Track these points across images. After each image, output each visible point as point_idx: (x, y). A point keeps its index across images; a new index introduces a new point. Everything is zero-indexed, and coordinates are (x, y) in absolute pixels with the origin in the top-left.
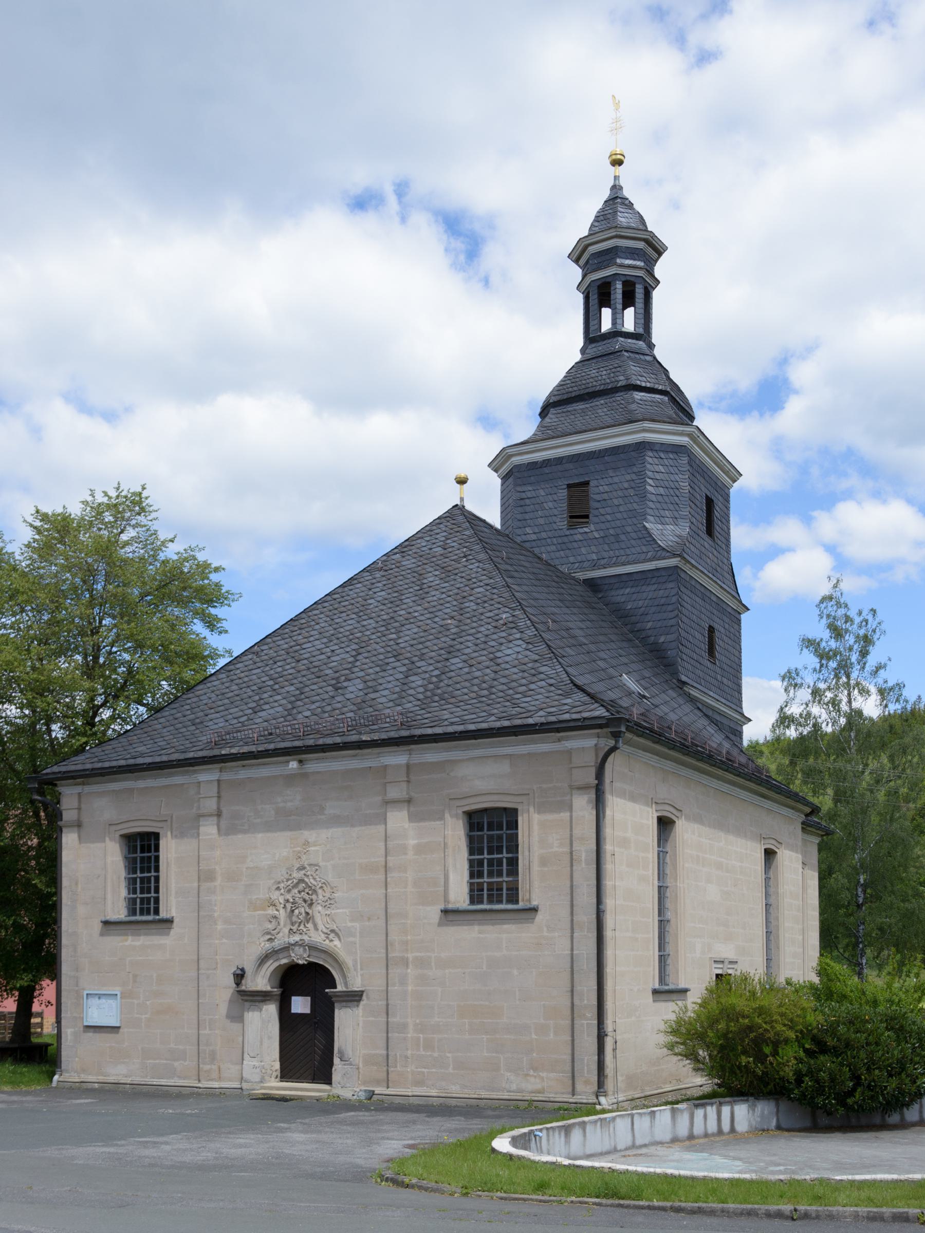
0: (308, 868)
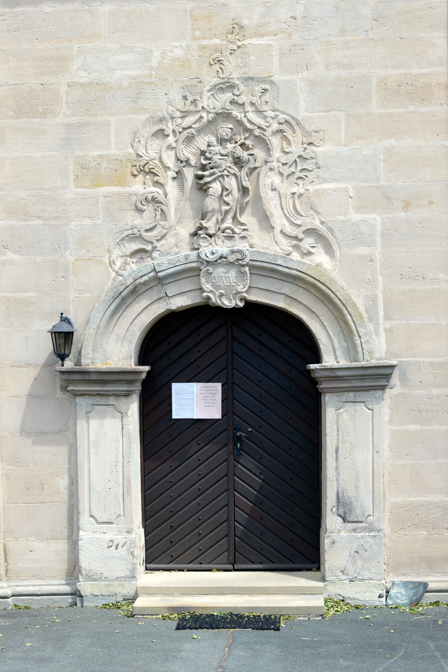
0: (242, 87)
